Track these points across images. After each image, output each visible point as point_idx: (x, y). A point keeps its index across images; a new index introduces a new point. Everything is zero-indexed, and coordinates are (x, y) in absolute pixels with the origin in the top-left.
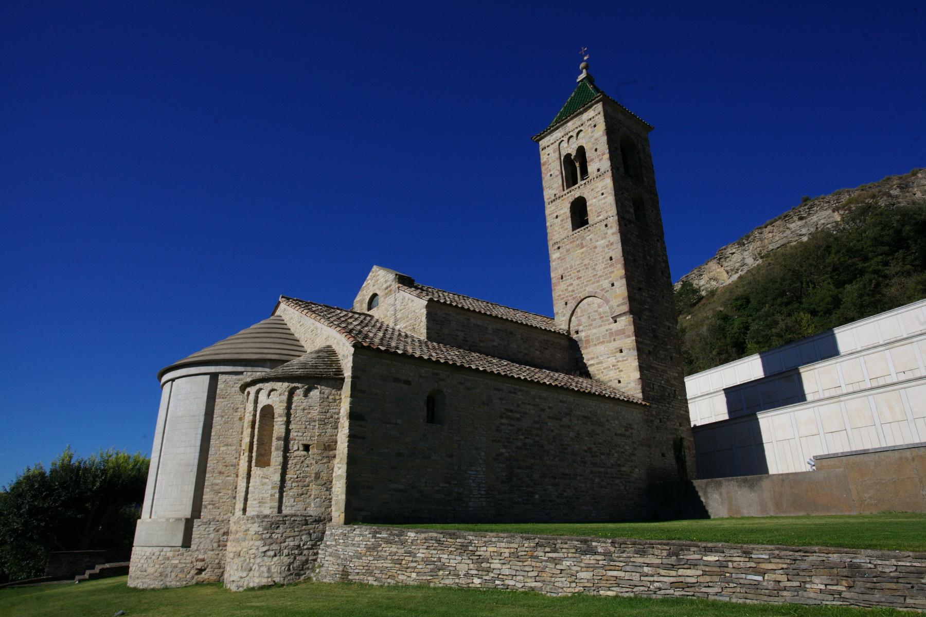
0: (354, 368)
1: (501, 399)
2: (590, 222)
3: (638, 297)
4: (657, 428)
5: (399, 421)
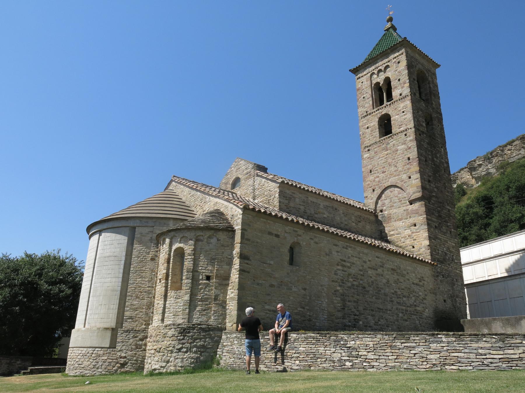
0: (243, 223)
1: (337, 252)
2: (393, 131)
3: (428, 187)
4: (441, 281)
5: (272, 262)
